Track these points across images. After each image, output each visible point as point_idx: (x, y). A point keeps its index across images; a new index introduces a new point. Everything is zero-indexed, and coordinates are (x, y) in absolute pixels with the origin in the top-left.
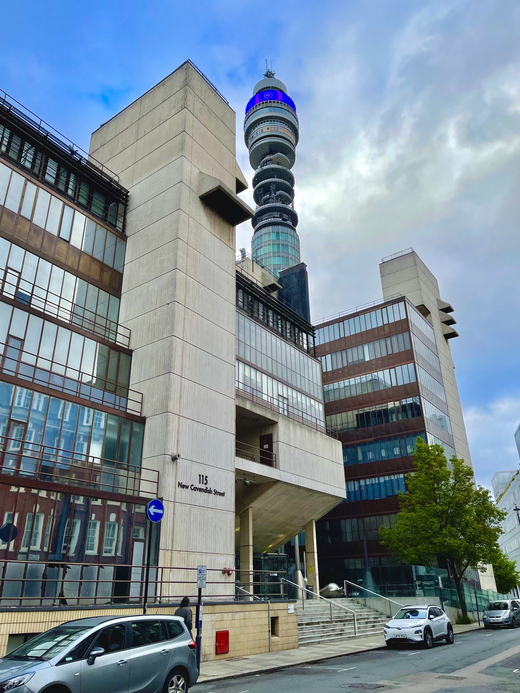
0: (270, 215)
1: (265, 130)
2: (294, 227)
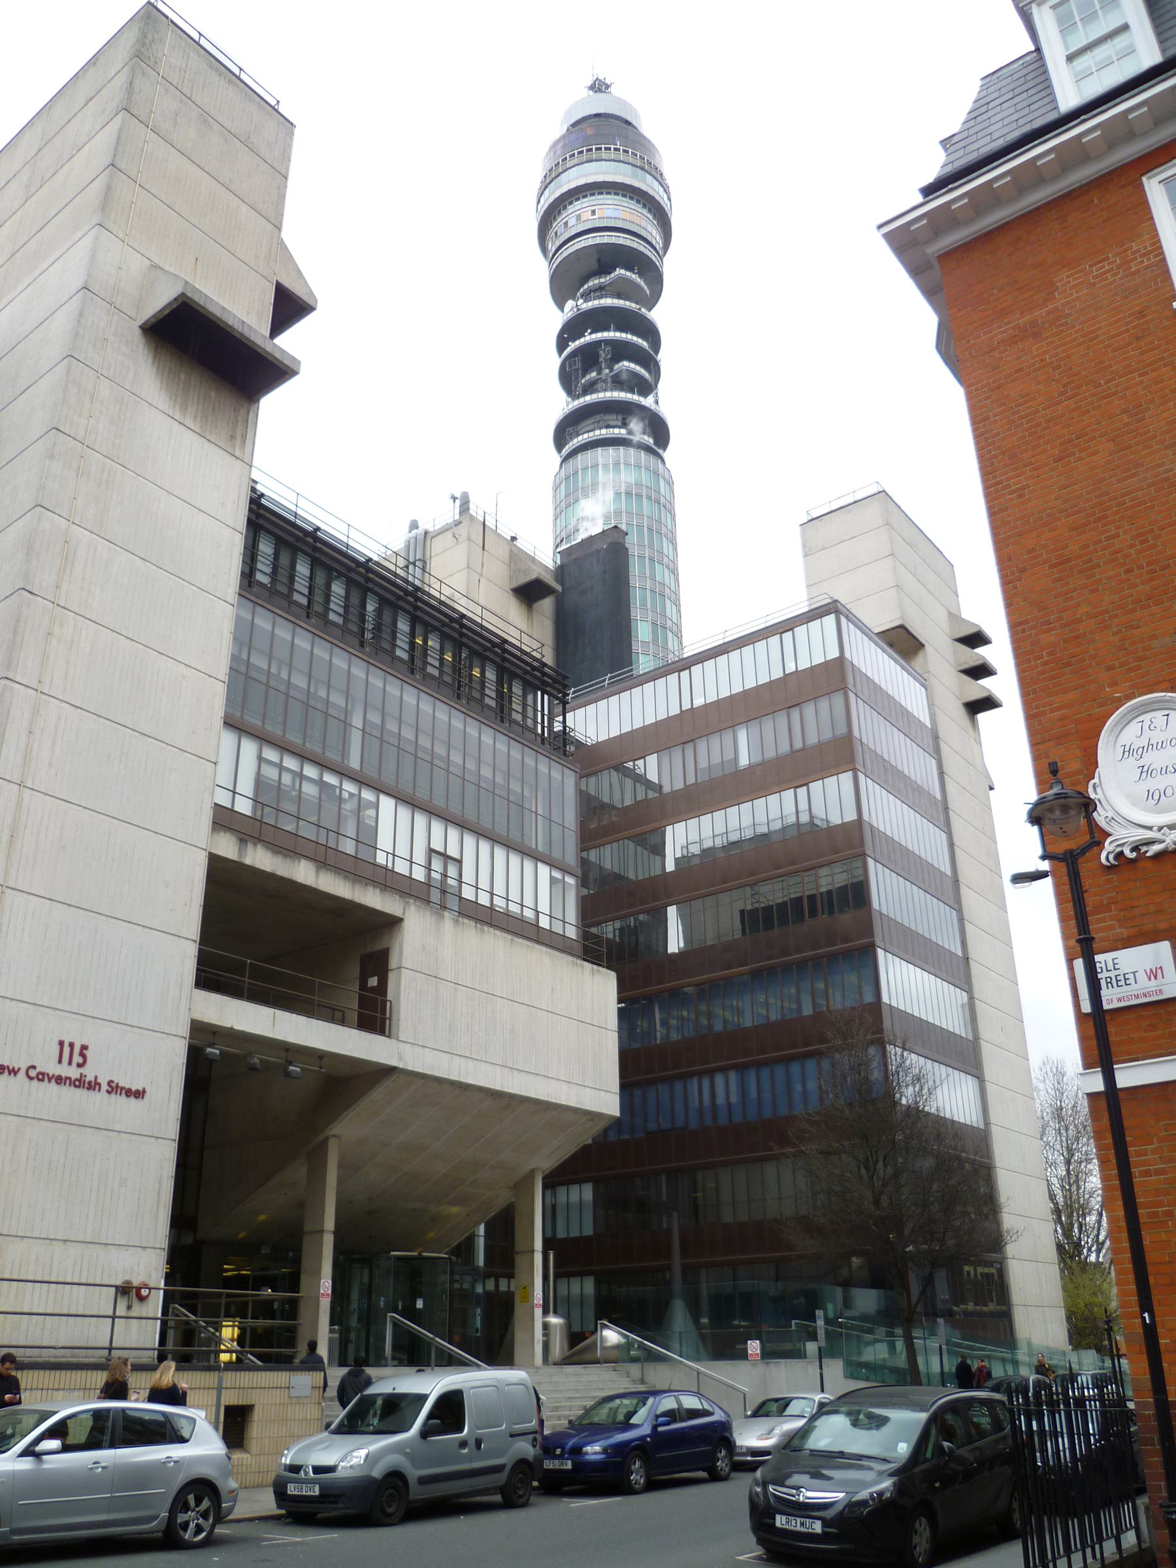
0: (599, 422)
1: (587, 215)
2: (660, 451)
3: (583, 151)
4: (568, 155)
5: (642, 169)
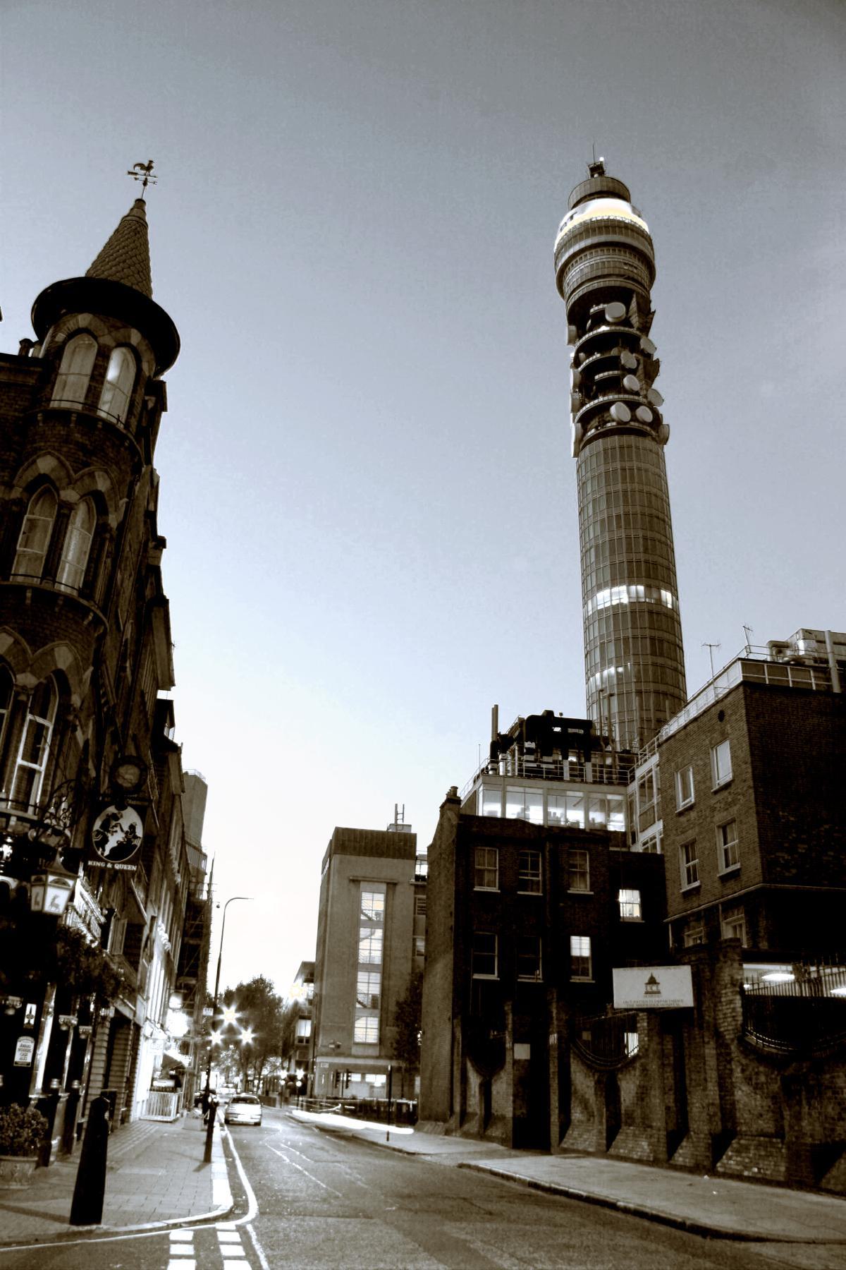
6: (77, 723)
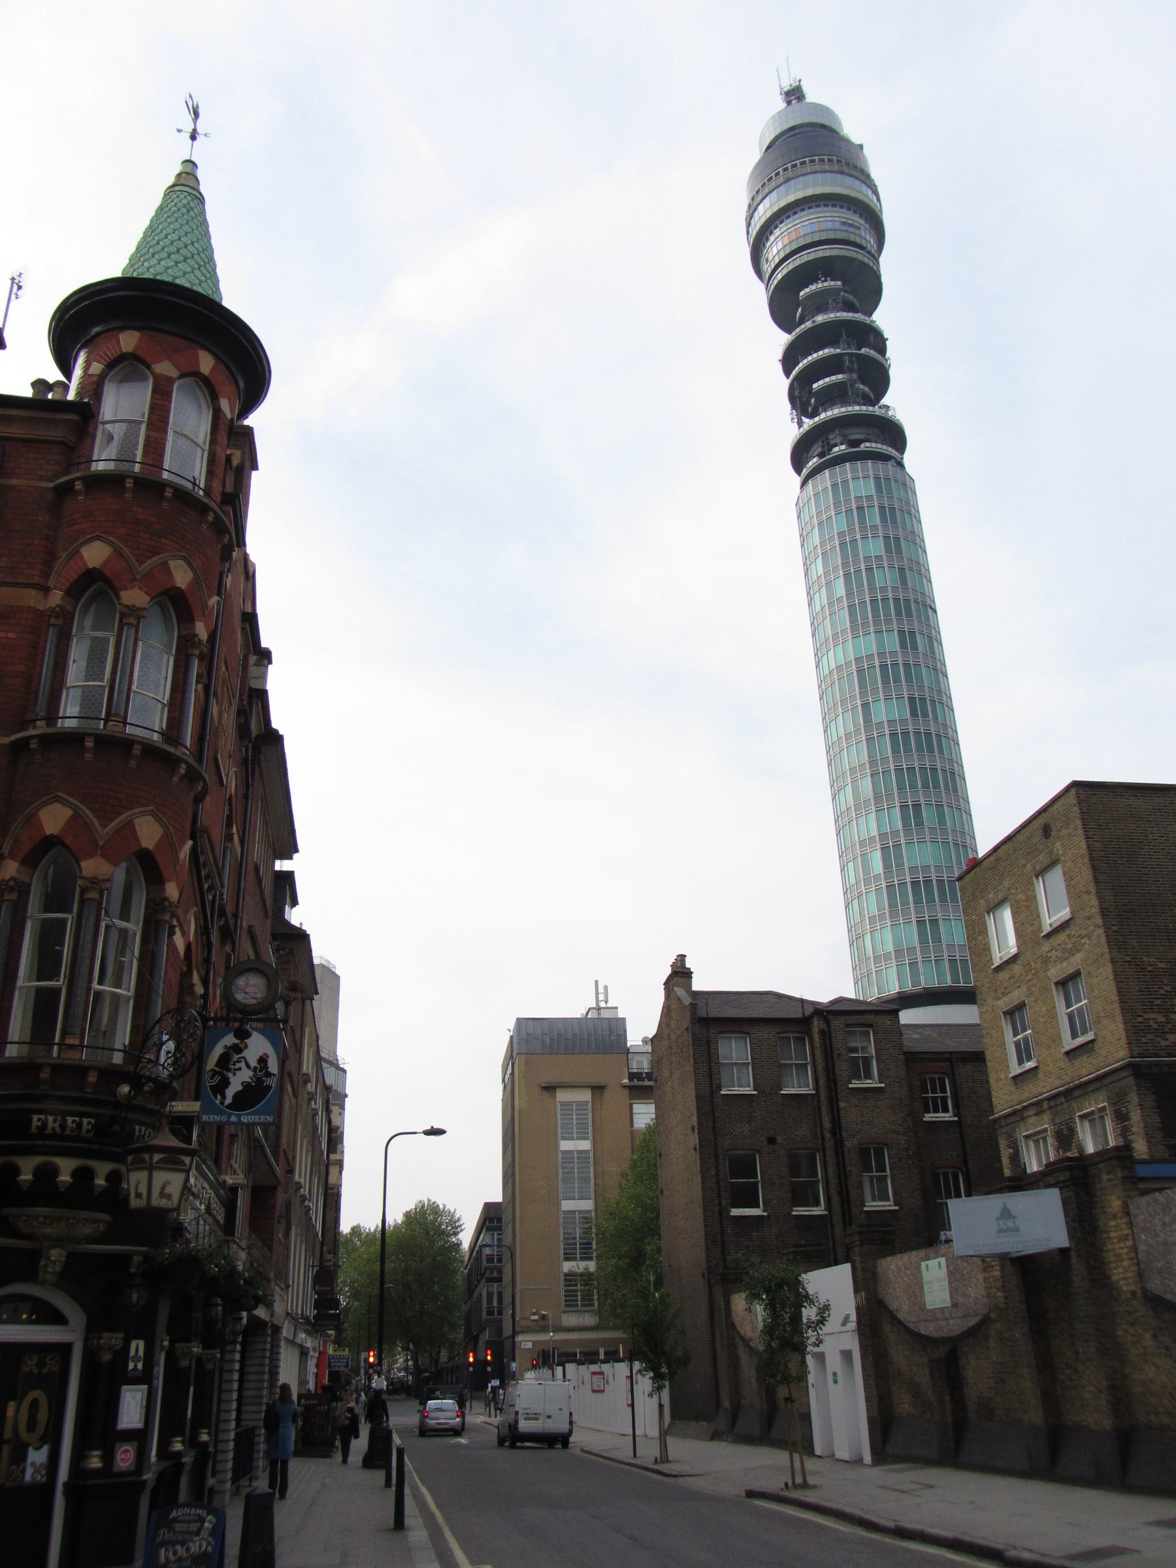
3: (788, 167)
4: (773, 174)
5: (842, 173)
6: (175, 923)
